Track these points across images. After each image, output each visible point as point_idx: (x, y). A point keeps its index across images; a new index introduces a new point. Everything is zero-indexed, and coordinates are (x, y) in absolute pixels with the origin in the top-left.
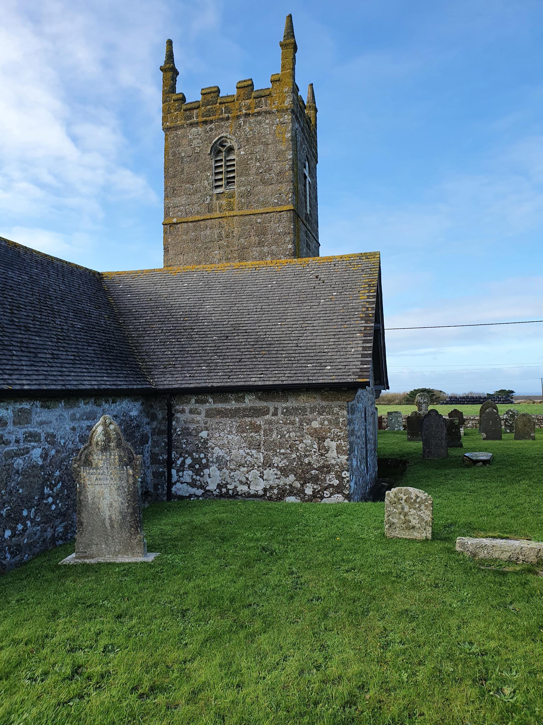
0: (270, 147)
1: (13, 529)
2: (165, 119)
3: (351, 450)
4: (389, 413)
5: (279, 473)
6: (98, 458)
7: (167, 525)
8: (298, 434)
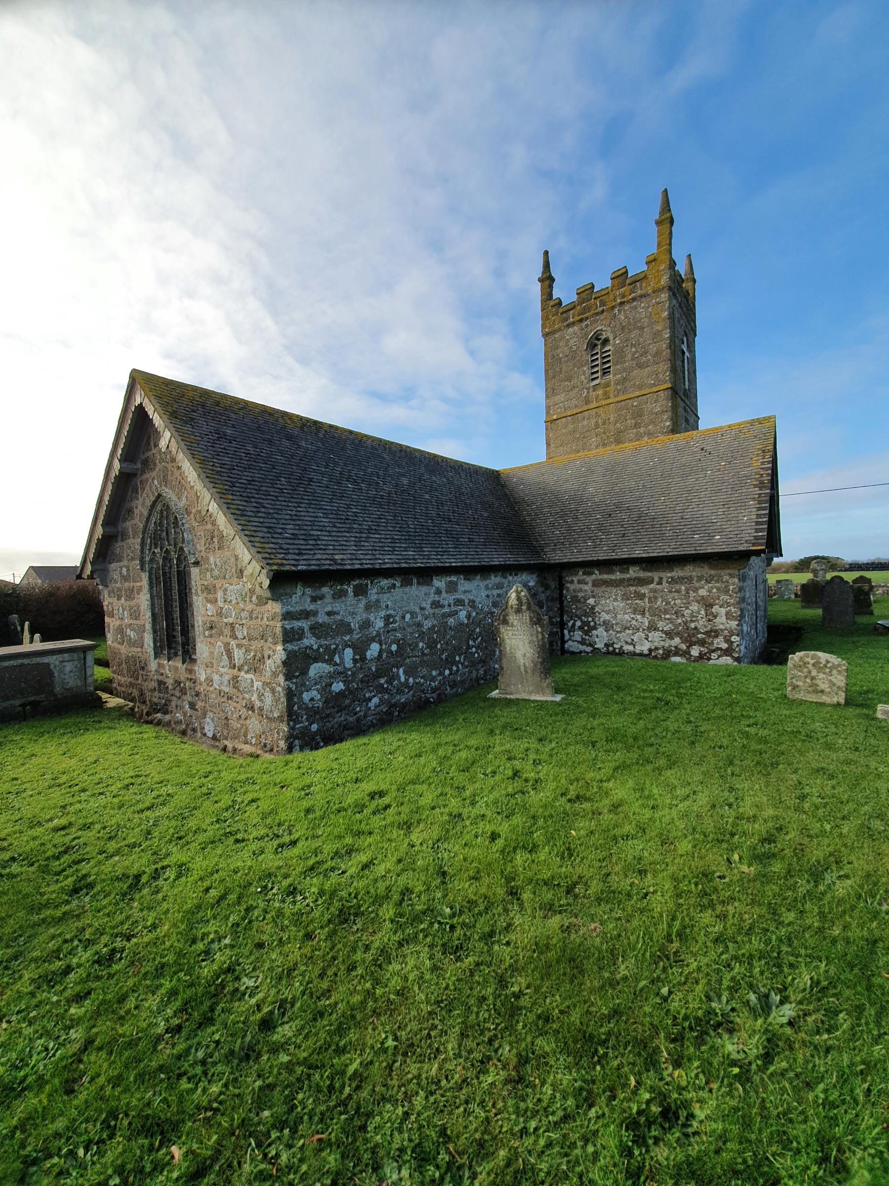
0: (645, 330)
1: (451, 670)
2: (544, 326)
3: (742, 616)
4: (778, 582)
5: (664, 636)
6: (513, 618)
7: (565, 673)
8: (684, 601)
